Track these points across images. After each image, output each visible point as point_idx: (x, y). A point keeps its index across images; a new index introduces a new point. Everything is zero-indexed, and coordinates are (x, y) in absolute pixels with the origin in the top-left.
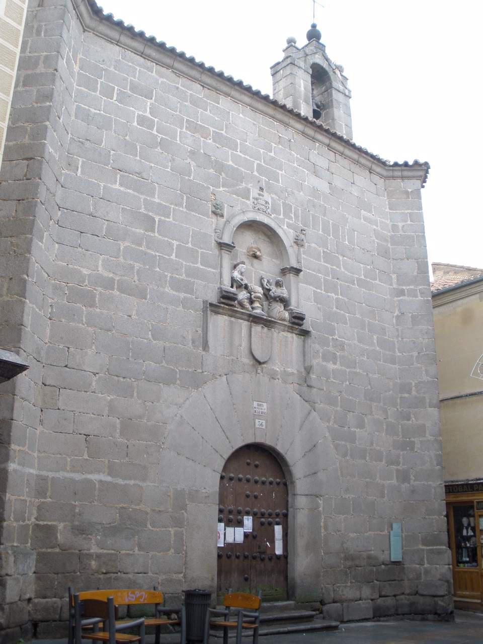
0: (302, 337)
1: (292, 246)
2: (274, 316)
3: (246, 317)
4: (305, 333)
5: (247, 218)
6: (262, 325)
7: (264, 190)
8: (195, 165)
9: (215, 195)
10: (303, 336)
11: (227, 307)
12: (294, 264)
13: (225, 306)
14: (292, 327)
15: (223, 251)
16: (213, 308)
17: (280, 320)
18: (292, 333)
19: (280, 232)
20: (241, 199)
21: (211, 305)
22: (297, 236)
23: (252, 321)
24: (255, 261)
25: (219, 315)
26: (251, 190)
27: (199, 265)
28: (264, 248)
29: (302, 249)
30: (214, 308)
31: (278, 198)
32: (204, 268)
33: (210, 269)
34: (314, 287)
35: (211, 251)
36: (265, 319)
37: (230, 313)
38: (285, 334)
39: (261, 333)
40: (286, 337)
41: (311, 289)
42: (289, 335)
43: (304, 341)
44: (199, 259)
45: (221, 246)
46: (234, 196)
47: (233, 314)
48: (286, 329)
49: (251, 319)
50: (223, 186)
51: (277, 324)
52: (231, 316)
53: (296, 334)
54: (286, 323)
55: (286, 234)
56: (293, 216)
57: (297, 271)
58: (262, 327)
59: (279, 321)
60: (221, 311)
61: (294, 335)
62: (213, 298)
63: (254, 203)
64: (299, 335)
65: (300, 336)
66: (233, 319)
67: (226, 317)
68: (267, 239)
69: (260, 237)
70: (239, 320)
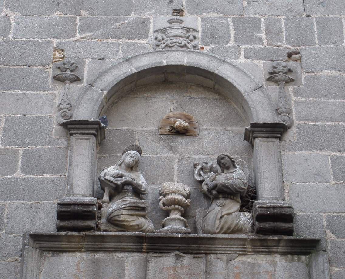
0: (303, 257)
1: (259, 88)
2: (209, 228)
3: (132, 245)
4: (308, 247)
5: (136, 68)
6: (177, 252)
7: (186, 12)
8: (19, 14)
9: (63, 51)
10: (305, 254)
11: (76, 234)
12: (265, 116)
13: (70, 233)
14: (261, 240)
15: (73, 138)
16: (44, 244)
17: (225, 233)
18: (270, 253)
19: (225, 71)
20: (127, 41)
21: (36, 237)
22: (275, 68)
23: (149, 251)
24: (181, 142)
25: (65, 254)
26: (151, 21)
27: (19, 174)
28: (202, 111)
29: (290, 89)
30: (44, 243)
31: (221, 15)
32: (31, 176)
33: (45, 176)
34: (333, 151)
35: (49, 144)
36: (182, 238)
37: (90, 244)
38: (249, 259)
39: (175, 268)
40: (253, 265)
41: (326, 156)
42: (262, 260)
43: (308, 265)
44: (20, 164)
45: (69, 130)
46: (110, 40)
47: (98, 244)
48: (249, 248)
49: (145, 245)
50: (82, 31)
51: (217, 242)
52: (95, 250)
53: (284, 254)
54: (244, 236)
55: (243, 70)
56: (263, 35)
57: (276, 130)
58: (178, 257)
59: (220, 236)
60: (65, 244)
61: (278, 258)
62: (47, 223)
63: (156, 39)
64: (292, 254)
65: (296, 258)
66: (100, 256)
67: (84, 256)
68: (210, 95)
69: (193, 96)
70: (117, 254)
